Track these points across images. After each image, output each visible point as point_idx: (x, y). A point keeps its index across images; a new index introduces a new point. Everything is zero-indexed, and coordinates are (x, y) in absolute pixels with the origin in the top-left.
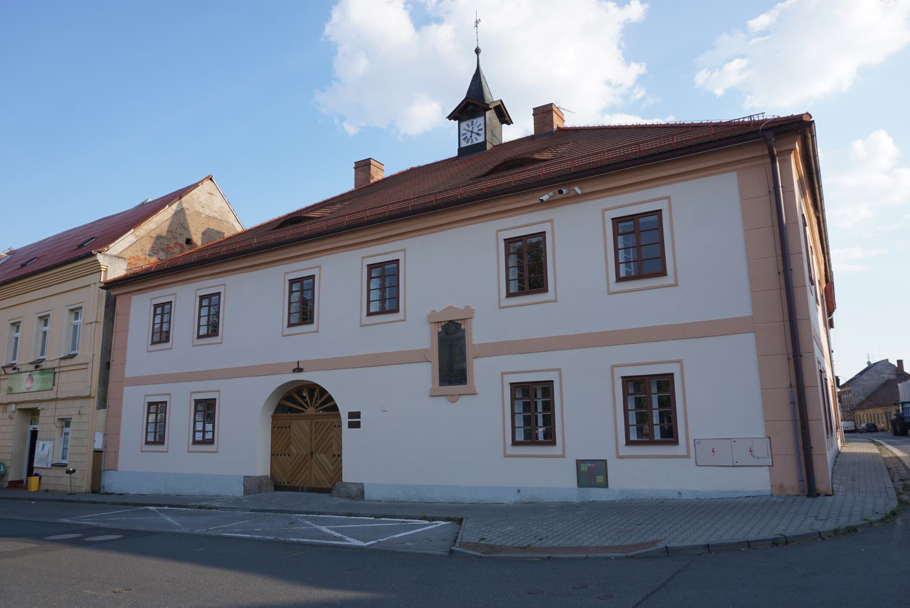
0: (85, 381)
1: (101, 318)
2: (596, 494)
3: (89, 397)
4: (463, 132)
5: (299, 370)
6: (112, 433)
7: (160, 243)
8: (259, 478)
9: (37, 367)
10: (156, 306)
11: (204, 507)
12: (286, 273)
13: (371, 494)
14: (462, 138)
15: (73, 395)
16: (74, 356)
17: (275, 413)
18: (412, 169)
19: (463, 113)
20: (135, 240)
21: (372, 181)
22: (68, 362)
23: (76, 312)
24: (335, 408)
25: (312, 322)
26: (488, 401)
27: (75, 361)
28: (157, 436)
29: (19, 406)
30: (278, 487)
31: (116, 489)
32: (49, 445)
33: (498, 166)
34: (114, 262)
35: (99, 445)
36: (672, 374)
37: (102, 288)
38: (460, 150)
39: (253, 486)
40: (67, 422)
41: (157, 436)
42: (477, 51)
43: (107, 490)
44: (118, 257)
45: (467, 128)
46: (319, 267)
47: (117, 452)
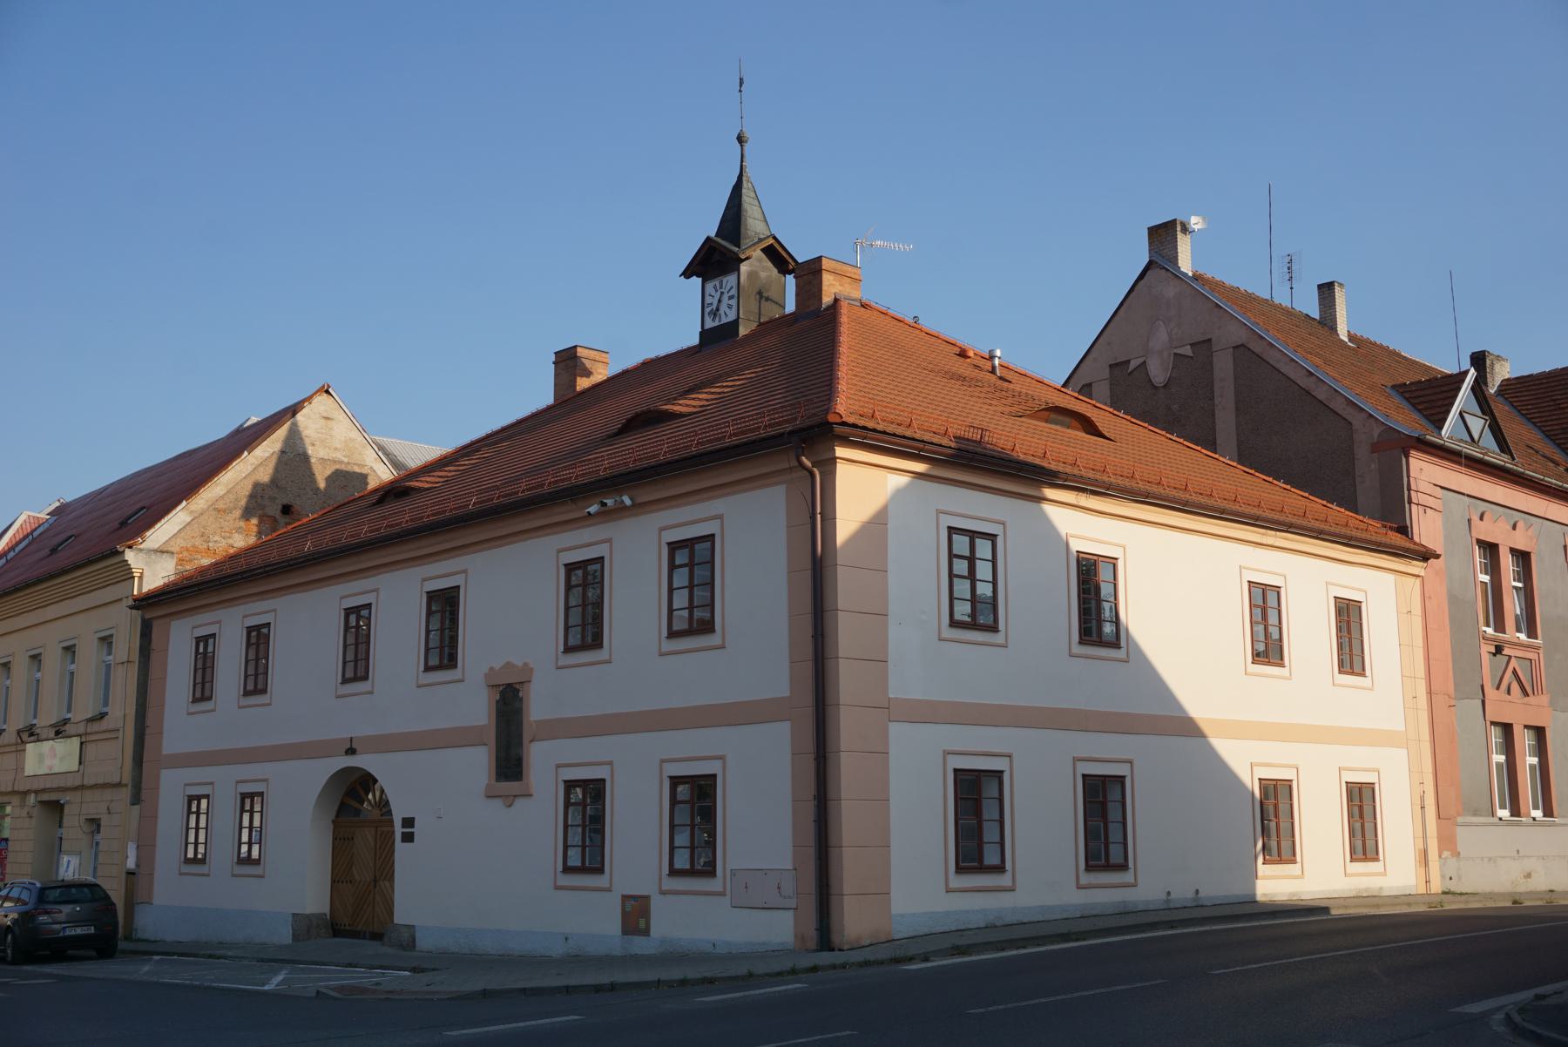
0: (113, 760)
1: (136, 657)
2: (640, 945)
3: (119, 785)
5: (351, 751)
6: (146, 847)
7: (258, 502)
8: (308, 916)
9: (58, 733)
12: (424, 580)
13: (424, 943)
15: (100, 781)
16: (102, 716)
17: (337, 815)
18: (647, 365)
19: (712, 262)
20: (189, 519)
21: (583, 383)
22: (95, 727)
23: (106, 641)
26: (541, 812)
27: (106, 724)
29: (46, 797)
30: (337, 930)
31: (148, 934)
32: (75, 861)
33: (630, 421)
34: (153, 562)
35: (131, 864)
36: (714, 776)
37: (131, 608)
38: (704, 334)
39: (305, 927)
40: (95, 824)
43: (141, 935)
44: (161, 551)
46: (376, 590)
47: (151, 874)
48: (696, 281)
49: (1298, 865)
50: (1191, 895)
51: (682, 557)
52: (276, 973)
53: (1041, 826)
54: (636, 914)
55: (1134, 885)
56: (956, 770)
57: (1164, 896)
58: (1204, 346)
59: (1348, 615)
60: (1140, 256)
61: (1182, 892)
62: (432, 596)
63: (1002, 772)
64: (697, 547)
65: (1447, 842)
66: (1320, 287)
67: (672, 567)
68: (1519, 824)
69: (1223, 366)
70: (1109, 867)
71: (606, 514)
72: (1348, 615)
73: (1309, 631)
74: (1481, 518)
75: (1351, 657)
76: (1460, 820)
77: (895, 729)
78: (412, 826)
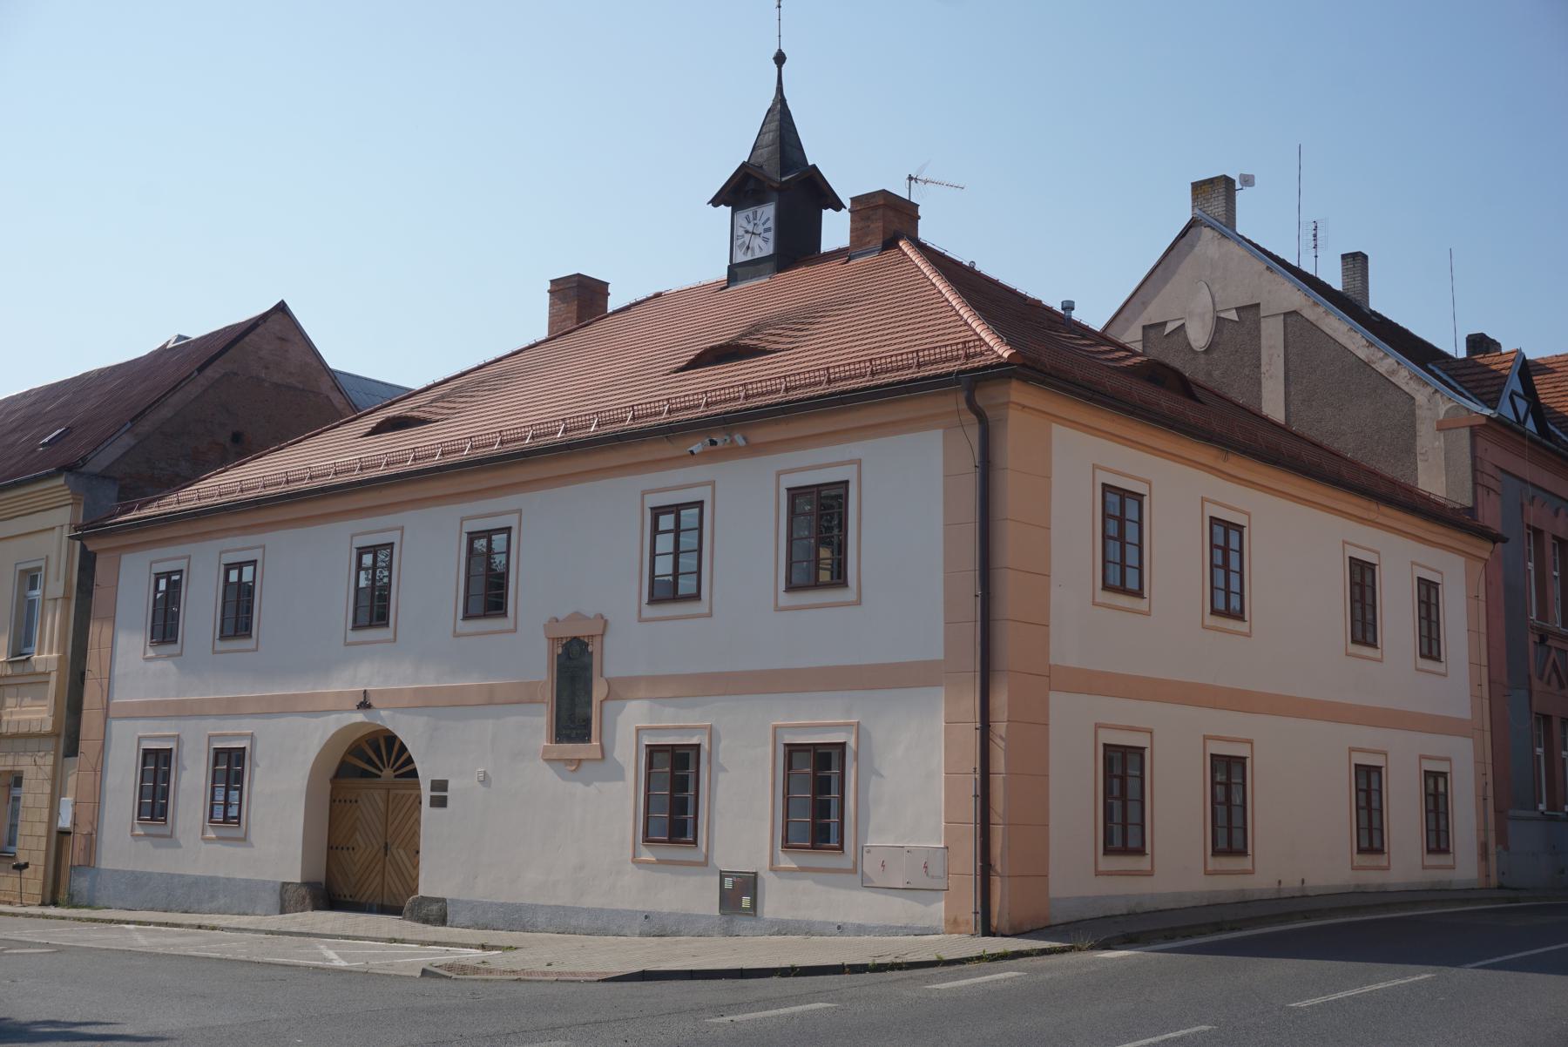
4: (739, 231)
6: (94, 803)
11: (206, 927)
12: (779, 474)
14: (737, 243)
20: (133, 443)
24: (414, 774)
28: (155, 802)
33: (699, 356)
38: (733, 269)
41: (155, 802)
42: (780, 59)
44: (103, 476)
45: (745, 223)
48: (725, 211)
49: (1148, 858)
50: (1298, 884)
53: (1177, 804)
54: (739, 894)
55: (1252, 872)
56: (1105, 745)
58: (1250, 311)
59: (1428, 594)
60: (1182, 211)
61: (1291, 883)
65: (1502, 837)
66: (1344, 257)
69: (1272, 335)
71: (714, 454)
72: (1428, 594)
76: (1511, 813)
77: (1057, 700)
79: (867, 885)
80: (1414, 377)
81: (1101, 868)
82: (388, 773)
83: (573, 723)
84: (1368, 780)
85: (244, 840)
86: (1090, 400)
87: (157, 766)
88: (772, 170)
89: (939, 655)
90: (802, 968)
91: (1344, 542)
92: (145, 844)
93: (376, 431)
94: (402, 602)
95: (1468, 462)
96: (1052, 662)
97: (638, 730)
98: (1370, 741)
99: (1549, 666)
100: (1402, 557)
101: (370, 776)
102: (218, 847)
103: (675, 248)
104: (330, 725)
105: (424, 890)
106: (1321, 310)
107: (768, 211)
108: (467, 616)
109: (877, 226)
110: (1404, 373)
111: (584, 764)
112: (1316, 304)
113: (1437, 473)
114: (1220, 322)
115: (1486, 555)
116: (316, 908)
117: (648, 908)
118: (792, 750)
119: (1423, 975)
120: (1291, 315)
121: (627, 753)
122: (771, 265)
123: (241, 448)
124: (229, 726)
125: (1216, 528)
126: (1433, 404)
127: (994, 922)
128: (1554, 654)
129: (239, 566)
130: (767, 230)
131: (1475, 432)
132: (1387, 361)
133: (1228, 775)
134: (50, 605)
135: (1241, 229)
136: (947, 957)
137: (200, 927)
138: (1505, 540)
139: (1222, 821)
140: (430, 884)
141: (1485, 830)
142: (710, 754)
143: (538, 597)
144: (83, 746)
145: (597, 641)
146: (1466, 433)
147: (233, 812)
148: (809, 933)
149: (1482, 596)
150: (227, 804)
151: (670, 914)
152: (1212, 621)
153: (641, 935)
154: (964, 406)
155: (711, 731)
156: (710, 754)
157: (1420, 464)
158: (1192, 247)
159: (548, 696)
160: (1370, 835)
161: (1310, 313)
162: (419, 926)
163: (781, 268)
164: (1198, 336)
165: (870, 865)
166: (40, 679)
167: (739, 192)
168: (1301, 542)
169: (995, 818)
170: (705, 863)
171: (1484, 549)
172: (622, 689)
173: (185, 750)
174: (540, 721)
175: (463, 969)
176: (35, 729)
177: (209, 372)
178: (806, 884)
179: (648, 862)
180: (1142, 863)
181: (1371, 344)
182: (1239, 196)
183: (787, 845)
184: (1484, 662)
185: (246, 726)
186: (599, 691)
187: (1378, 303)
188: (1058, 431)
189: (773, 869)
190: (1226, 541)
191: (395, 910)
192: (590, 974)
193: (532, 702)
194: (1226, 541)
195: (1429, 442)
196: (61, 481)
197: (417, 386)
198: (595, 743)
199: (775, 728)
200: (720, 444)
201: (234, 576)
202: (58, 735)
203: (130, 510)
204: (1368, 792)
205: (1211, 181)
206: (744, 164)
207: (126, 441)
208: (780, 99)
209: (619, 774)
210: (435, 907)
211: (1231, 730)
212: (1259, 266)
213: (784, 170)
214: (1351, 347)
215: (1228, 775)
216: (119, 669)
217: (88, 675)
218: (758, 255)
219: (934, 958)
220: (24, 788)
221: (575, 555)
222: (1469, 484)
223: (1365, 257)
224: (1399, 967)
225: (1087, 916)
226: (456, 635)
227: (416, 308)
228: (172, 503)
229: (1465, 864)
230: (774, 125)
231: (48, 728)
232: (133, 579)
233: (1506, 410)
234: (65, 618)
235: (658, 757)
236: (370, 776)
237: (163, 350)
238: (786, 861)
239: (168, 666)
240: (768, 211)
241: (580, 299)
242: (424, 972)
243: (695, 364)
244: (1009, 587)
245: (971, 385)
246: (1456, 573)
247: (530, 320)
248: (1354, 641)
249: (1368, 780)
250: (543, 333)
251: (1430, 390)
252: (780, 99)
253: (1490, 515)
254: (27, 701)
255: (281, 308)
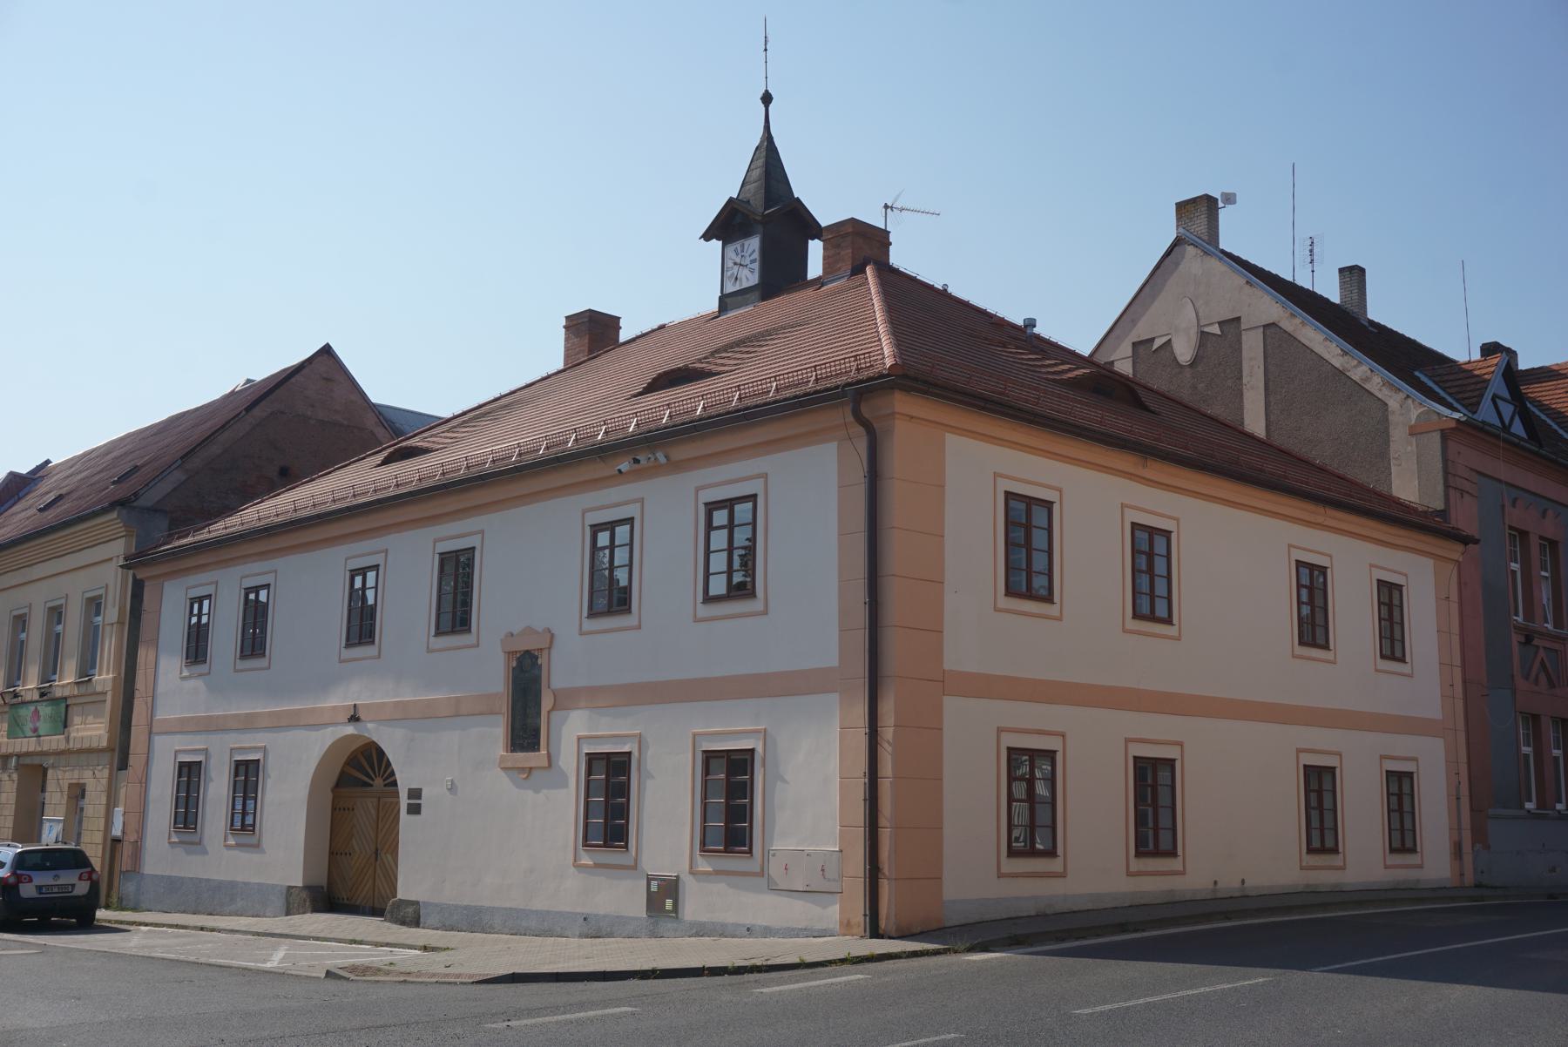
4: (729, 264)
6: (140, 814)
9: (42, 695)
10: (711, 507)
12: (697, 490)
20: (184, 478)
24: (395, 783)
25: (469, 631)
41: (187, 816)
42: (767, 99)
44: (154, 510)
46: (642, 500)
48: (716, 245)
50: (1237, 884)
51: (720, 517)
52: (275, 948)
53: (1095, 809)
54: (663, 897)
55: (1183, 873)
56: (1009, 749)
57: (1211, 886)
58: (1232, 325)
59: (1390, 597)
60: (1168, 232)
61: (1229, 882)
62: (445, 558)
63: (1054, 752)
64: (737, 508)
65: (1479, 835)
66: (1341, 270)
67: (710, 527)
68: (1544, 817)
69: (1252, 346)
70: (1157, 853)
71: (639, 474)
72: (1390, 597)
73: (1353, 613)
74: (1514, 505)
75: (1392, 644)
76: (1491, 812)
77: (951, 704)
78: (419, 797)
79: (773, 889)
80: (1387, 384)
81: (1004, 870)
82: (378, 782)
83: (525, 734)
84: (1319, 783)
85: (257, 846)
86: (983, 409)
87: (190, 774)
88: (757, 203)
89: (835, 663)
90: (663, 971)
91: (1290, 546)
92: (179, 851)
93: (385, 462)
94: (387, 624)
95: (1440, 465)
96: (947, 666)
97: (579, 739)
98: (1322, 743)
99: (1537, 664)
100: (1357, 562)
101: (360, 783)
102: (236, 853)
103: (673, 282)
104: (329, 736)
105: (401, 894)
106: (1298, 321)
107: (754, 244)
108: (439, 632)
109: (847, 253)
110: (1377, 380)
111: (535, 773)
112: (1292, 315)
113: (1410, 481)
114: (1203, 335)
115: (1456, 556)
116: (316, 910)
117: (586, 910)
118: (709, 756)
119: (1258, 978)
120: (1270, 327)
121: (570, 761)
122: (756, 294)
123: (288, 477)
124: (248, 740)
125: (1138, 533)
126: (1406, 409)
127: (882, 924)
128: (1542, 653)
129: (256, 589)
130: (753, 261)
131: (1445, 435)
132: (1361, 369)
133: (1153, 783)
134: (108, 629)
135: (1224, 244)
136: (809, 959)
137: (202, 929)
138: (1476, 542)
139: (1315, 823)
140: (408, 888)
141: (1460, 829)
142: (639, 761)
143: (499, 608)
144: (132, 760)
145: (545, 653)
146: (1437, 437)
147: (249, 820)
148: (722, 935)
149: (1454, 596)
150: (244, 813)
151: (605, 916)
152: (1132, 624)
153: (581, 936)
154: (850, 418)
155: (640, 739)
156: (639, 761)
157: (1393, 469)
158: (1177, 264)
159: (504, 709)
160: (1322, 832)
161: (1288, 325)
162: (395, 927)
163: (764, 298)
164: (1184, 351)
165: (775, 869)
166: (97, 699)
167: (728, 225)
168: (1236, 549)
169: (884, 821)
170: (635, 867)
171: (1455, 551)
172: (568, 699)
173: (212, 761)
174: (497, 731)
175: (366, 970)
176: (94, 745)
177: (256, 412)
178: (720, 887)
179: (586, 866)
180: (1055, 865)
181: (1345, 353)
182: (1222, 214)
183: (704, 848)
184: (1457, 661)
185: (260, 739)
186: (546, 702)
187: (1379, 310)
188: (952, 440)
189: (692, 872)
190: (1150, 553)
191: (376, 912)
192: (471, 976)
193: (492, 713)
194: (1150, 553)
195: (1402, 447)
196: (114, 515)
197: (448, 415)
198: (543, 752)
199: (695, 735)
200: (643, 462)
201: (252, 596)
202: (113, 750)
203: (186, 536)
204: (1400, 796)
205: (1194, 201)
206: (731, 200)
207: (178, 476)
208: (768, 137)
209: (565, 785)
210: (410, 910)
211: (1156, 733)
212: (1238, 279)
213: (769, 200)
214: (1326, 356)
215: (1153, 783)
216: (161, 689)
217: (137, 694)
218: (745, 285)
219: (797, 960)
220: (86, 800)
221: (531, 567)
222: (1440, 488)
223: (1362, 271)
224: (1250, 970)
225: (987, 917)
226: (429, 651)
227: (450, 346)
228: (219, 528)
229: (1435, 862)
230: (761, 162)
231: (104, 744)
232: (170, 606)
233: (1486, 413)
234: (120, 639)
235: (714, 763)
236: (360, 783)
237: (233, 393)
238: (704, 865)
239: (198, 684)
240: (754, 244)
241: (593, 333)
242: (329, 974)
243: (1146, 409)
244: (895, 594)
245: (854, 400)
246: (1424, 578)
247: (550, 354)
248: (1301, 643)
249: (1319, 783)
250: (559, 364)
251: (1402, 395)
252: (768, 137)
253: (1465, 517)
254: (90, 718)
255: (327, 351)
